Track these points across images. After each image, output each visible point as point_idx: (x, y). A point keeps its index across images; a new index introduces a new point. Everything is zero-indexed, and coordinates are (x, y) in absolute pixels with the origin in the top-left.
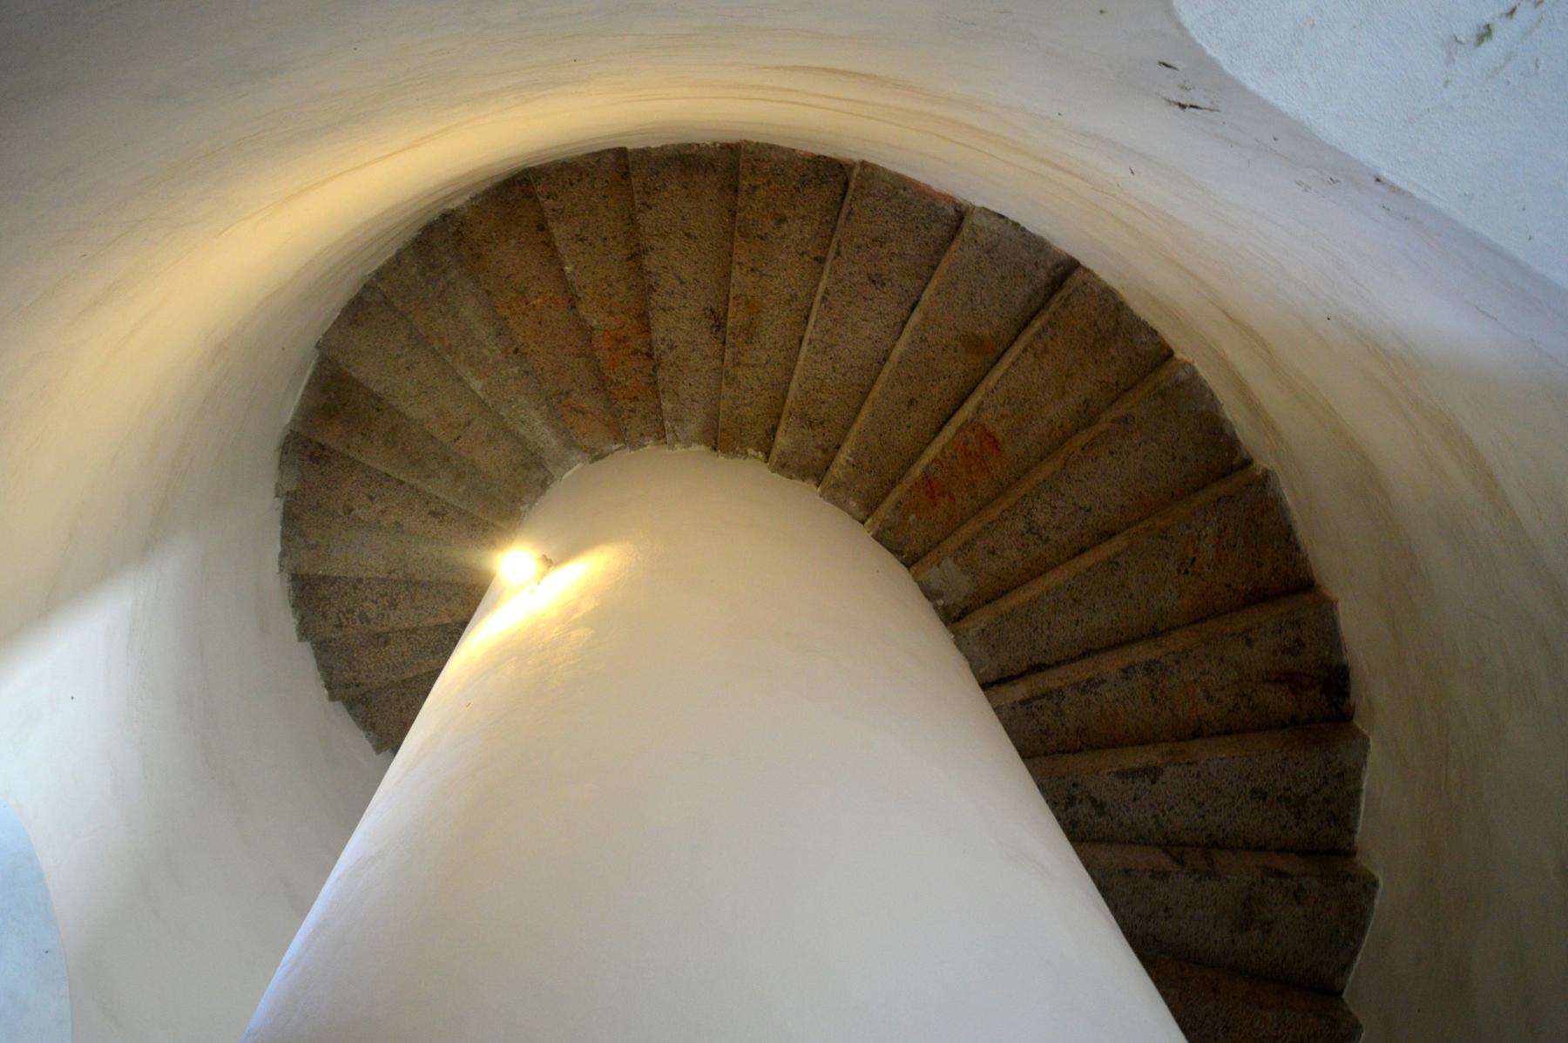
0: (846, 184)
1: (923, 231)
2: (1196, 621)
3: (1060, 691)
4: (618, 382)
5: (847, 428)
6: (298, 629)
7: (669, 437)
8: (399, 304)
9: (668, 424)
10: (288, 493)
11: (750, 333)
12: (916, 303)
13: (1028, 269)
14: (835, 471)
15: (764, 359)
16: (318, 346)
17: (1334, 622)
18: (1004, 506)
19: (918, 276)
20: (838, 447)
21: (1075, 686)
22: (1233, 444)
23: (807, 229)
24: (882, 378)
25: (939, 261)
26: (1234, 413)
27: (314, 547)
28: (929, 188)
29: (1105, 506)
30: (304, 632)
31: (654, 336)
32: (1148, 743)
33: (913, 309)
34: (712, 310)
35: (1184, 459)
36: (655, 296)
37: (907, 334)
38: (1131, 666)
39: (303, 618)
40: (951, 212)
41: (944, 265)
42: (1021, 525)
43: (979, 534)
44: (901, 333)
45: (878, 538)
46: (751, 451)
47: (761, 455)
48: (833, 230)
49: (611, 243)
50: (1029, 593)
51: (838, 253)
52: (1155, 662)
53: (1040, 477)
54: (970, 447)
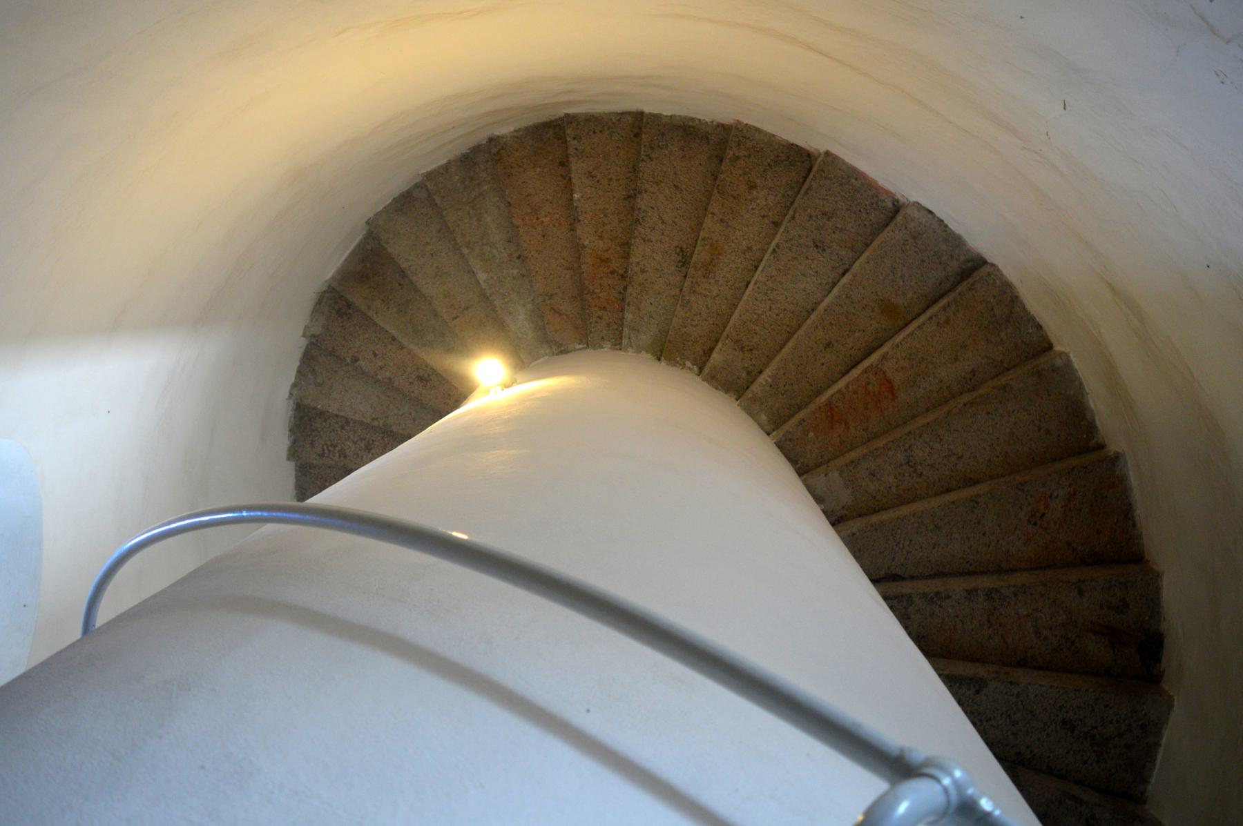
0: (810, 170)
1: (864, 215)
2: (1036, 569)
3: (910, 596)
4: (593, 293)
5: (770, 359)
6: (290, 449)
7: (625, 342)
8: (438, 201)
9: (626, 331)
10: (313, 336)
11: (709, 268)
12: (847, 270)
13: (945, 258)
14: (755, 388)
15: (715, 292)
16: (368, 222)
17: (1158, 591)
18: (890, 439)
19: (853, 249)
20: (760, 372)
21: (924, 595)
22: (1092, 428)
23: (771, 198)
24: (809, 322)
25: (872, 241)
26: (1098, 402)
27: (320, 385)
28: (876, 182)
29: (975, 457)
30: (293, 453)
31: (633, 259)
32: (978, 660)
33: (844, 274)
34: (682, 250)
35: (1048, 432)
36: (639, 228)
37: (835, 290)
38: (976, 589)
39: (295, 441)
40: (889, 205)
41: (876, 243)
42: (901, 457)
43: (865, 457)
44: (830, 292)
45: (780, 446)
46: (688, 364)
47: (695, 368)
48: (792, 203)
49: (615, 184)
50: (897, 513)
51: (793, 218)
52: (997, 590)
53: (925, 421)
54: (870, 387)
